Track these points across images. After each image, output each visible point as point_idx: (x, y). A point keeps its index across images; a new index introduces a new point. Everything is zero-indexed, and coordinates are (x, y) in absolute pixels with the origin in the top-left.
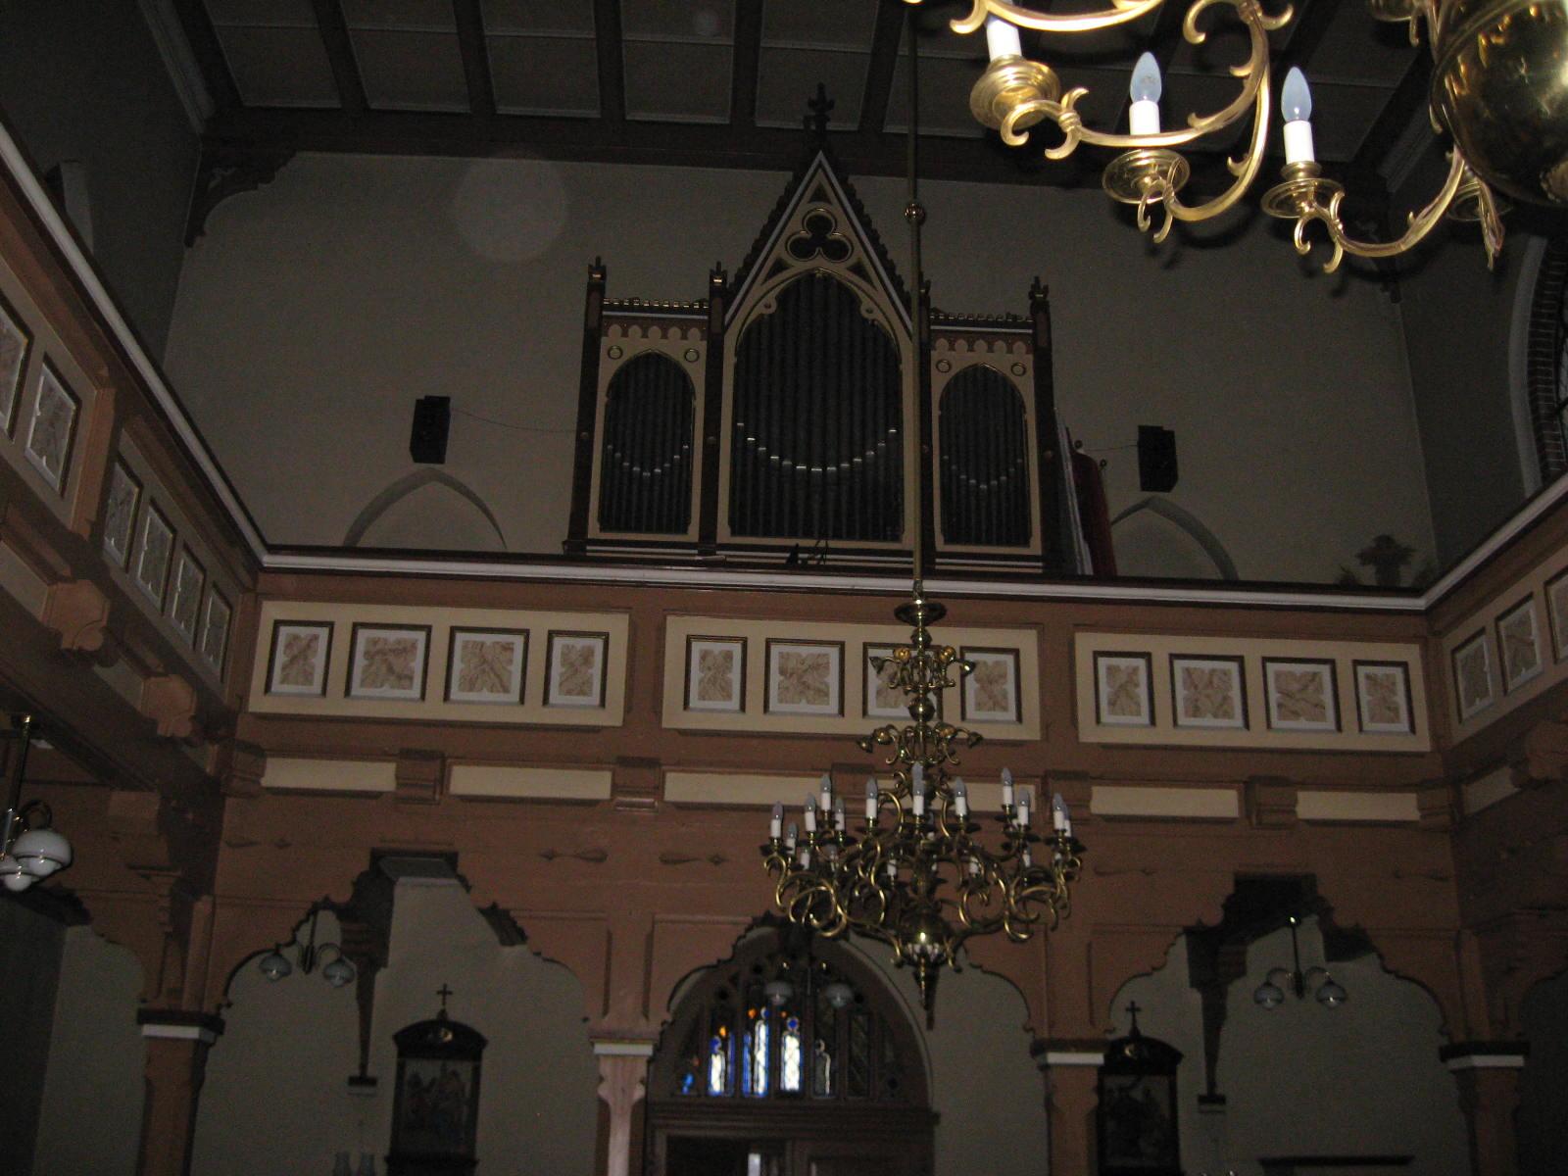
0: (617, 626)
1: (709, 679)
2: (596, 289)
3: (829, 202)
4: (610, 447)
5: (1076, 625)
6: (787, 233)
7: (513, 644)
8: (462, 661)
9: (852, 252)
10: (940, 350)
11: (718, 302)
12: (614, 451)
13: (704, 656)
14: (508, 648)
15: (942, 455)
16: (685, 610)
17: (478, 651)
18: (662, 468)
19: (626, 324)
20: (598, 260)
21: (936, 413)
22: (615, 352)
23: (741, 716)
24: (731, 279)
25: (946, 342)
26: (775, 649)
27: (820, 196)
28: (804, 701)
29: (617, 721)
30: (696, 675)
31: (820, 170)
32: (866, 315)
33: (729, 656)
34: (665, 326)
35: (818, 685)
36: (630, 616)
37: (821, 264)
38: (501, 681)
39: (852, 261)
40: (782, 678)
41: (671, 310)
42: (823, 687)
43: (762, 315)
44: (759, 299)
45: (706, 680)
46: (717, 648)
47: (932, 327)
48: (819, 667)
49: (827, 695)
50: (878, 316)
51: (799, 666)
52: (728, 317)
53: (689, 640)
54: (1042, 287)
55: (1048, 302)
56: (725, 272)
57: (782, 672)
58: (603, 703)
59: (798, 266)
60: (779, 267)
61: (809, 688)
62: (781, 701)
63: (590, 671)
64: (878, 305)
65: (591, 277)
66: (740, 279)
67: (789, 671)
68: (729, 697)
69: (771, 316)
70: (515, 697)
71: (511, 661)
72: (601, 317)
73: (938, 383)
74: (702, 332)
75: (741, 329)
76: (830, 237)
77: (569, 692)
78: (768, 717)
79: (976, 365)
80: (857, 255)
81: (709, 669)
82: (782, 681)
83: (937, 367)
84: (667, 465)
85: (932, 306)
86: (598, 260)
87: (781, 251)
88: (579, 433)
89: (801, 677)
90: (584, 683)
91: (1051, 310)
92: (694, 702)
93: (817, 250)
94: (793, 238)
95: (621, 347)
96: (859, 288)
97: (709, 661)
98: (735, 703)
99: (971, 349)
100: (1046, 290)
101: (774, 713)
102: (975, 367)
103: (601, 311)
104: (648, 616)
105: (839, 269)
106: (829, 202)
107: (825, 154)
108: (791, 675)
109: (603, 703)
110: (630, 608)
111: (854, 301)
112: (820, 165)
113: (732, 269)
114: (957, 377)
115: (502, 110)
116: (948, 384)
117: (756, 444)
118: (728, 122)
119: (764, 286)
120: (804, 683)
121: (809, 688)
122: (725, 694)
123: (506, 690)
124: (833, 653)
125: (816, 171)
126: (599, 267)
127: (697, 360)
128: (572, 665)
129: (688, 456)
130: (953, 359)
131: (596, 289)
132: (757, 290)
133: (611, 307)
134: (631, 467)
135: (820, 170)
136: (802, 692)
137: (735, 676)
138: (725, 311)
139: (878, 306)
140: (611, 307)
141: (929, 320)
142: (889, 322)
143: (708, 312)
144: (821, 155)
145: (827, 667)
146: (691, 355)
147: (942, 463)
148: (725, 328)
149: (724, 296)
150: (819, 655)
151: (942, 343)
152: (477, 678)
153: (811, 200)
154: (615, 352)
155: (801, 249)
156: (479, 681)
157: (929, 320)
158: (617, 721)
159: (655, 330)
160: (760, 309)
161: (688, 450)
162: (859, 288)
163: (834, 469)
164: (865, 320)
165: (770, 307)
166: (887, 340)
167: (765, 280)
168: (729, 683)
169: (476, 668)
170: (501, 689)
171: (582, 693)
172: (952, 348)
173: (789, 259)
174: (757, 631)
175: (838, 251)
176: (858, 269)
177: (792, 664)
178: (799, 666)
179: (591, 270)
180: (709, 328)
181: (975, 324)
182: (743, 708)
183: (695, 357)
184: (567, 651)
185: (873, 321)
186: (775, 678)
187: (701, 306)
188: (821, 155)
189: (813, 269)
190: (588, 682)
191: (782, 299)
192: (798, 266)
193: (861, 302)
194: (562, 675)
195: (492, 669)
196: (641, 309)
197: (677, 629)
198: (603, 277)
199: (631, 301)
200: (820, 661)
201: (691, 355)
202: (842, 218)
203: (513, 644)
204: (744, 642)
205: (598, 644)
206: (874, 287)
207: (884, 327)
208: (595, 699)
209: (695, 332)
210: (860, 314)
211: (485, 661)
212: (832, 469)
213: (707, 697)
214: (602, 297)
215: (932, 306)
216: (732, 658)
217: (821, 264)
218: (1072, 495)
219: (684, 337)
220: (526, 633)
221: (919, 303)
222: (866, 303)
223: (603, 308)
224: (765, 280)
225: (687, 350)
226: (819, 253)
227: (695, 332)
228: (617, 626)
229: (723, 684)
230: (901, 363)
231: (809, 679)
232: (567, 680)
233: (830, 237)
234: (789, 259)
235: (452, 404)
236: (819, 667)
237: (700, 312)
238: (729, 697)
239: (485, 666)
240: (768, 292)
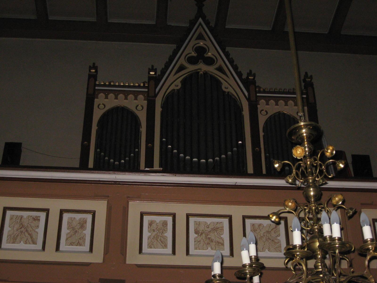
0: (100, 207)
1: (154, 237)
2: (93, 77)
3: (205, 40)
4: (98, 150)
5: (362, 204)
6: (186, 52)
7: (40, 217)
8: (9, 226)
9: (216, 63)
10: (262, 105)
11: (152, 83)
12: (101, 152)
13: (151, 224)
14: (37, 219)
15: (265, 154)
16: (139, 197)
17: (19, 221)
18: (125, 160)
19: (107, 93)
20: (94, 64)
21: (262, 134)
22: (102, 106)
23: (173, 257)
24: (159, 73)
25: (264, 101)
26: (192, 219)
27: (200, 37)
28: (209, 248)
29: (100, 260)
30: (146, 234)
31: (200, 26)
32: (224, 89)
33: (165, 224)
34: (126, 94)
35: (217, 239)
36: (108, 201)
37: (202, 67)
38: (32, 237)
39: (217, 66)
40: (196, 235)
41: (129, 86)
42: (221, 241)
43: (174, 90)
44: (172, 82)
45: (152, 237)
46: (158, 219)
47: (258, 95)
48: (217, 229)
49: (223, 244)
50: (230, 90)
51: (206, 229)
52: (157, 90)
53: (142, 215)
54: (309, 76)
55: (312, 83)
56: (156, 69)
57: (196, 232)
58: (91, 250)
59: (191, 68)
60: (182, 68)
61: (212, 242)
62: (196, 249)
63: (84, 232)
64: (231, 85)
65: (90, 71)
66: (163, 72)
67: (201, 232)
68: (166, 246)
69: (178, 90)
70: (40, 247)
71: (38, 227)
72: (95, 89)
73: (262, 120)
74: (144, 96)
75: (166, 92)
76: (206, 55)
77: (71, 244)
78: (189, 258)
79: (280, 112)
80: (220, 62)
81: (154, 231)
82: (197, 237)
83: (261, 113)
84: (127, 159)
85: (257, 85)
86: (94, 64)
87: (182, 61)
88: (82, 142)
89: (208, 235)
90: (80, 239)
91: (314, 86)
92: (145, 249)
93: (200, 60)
94: (188, 56)
95: (104, 104)
96: (221, 77)
97: (154, 226)
98: (169, 250)
99: (277, 104)
100: (311, 77)
101: (192, 255)
102: (279, 113)
103: (95, 87)
104: (118, 201)
105: (211, 69)
106: (205, 40)
107: (202, 19)
108: (202, 234)
109: (91, 250)
110: (108, 196)
111: (219, 84)
112: (200, 24)
113: (160, 67)
114: (270, 117)
115: (50, 18)
116: (267, 120)
117: (172, 149)
118: (154, 23)
119: (175, 76)
120: (209, 238)
121: (212, 242)
122: (163, 245)
123: (34, 243)
124: (226, 221)
125: (198, 27)
126: (94, 67)
127: (142, 109)
128: (73, 229)
129: (138, 155)
130: (267, 109)
131: (93, 77)
132: (172, 78)
133: (100, 85)
134: (109, 160)
135: (200, 26)
136: (208, 244)
137: (169, 234)
138: (156, 88)
139: (231, 86)
140: (100, 85)
141: (256, 91)
142: (235, 91)
143: (148, 87)
144: (200, 20)
145: (222, 229)
146: (139, 108)
147: (266, 158)
148: (156, 95)
149: (156, 80)
150: (217, 223)
151: (262, 101)
152: (18, 236)
153: (197, 39)
154: (102, 106)
155: (192, 61)
156: (19, 237)
157: (256, 91)
158: (100, 260)
159: (121, 96)
160: (173, 87)
161: (138, 151)
162: (221, 77)
163: (211, 160)
164: (224, 92)
165: (178, 86)
166: (235, 100)
167: (175, 74)
168: (165, 238)
169: (17, 230)
170: (31, 242)
171: (79, 244)
172: (267, 104)
173: (186, 64)
174: (181, 209)
175: (210, 61)
176: (220, 69)
177: (201, 228)
178: (206, 229)
179: (90, 68)
180: (148, 96)
181: (279, 93)
182: (174, 252)
183: (142, 108)
184: (71, 220)
185: (228, 92)
186: (192, 235)
187: (144, 84)
188: (200, 20)
189: (198, 69)
190: (83, 238)
191: (184, 82)
192: (191, 68)
193: (222, 84)
194: (67, 234)
195: (27, 231)
196: (115, 86)
197: (135, 208)
198: (96, 71)
199: (110, 83)
200: (218, 226)
201: (139, 108)
202: (211, 46)
203: (40, 217)
204: (174, 216)
205: (89, 217)
206: (227, 76)
207: (234, 95)
208: (87, 248)
209: (141, 97)
210: (222, 89)
211: (23, 226)
212: (211, 160)
213: (153, 246)
214: (96, 80)
215: (257, 85)
216: (167, 225)
217: (202, 67)
218: (332, 171)
219: (136, 99)
220: (47, 211)
221: (249, 83)
222: (224, 85)
223: (95, 85)
224: (175, 74)
225: (137, 105)
226: (201, 62)
227: (141, 97)
228: (100, 207)
229: (162, 239)
230: (243, 111)
231: (212, 236)
232: (71, 236)
233: (206, 55)
234: (186, 64)
235: (23, 146)
236: (217, 229)
237: (144, 87)
238: (166, 246)
239: (23, 229)
240: (176, 79)
